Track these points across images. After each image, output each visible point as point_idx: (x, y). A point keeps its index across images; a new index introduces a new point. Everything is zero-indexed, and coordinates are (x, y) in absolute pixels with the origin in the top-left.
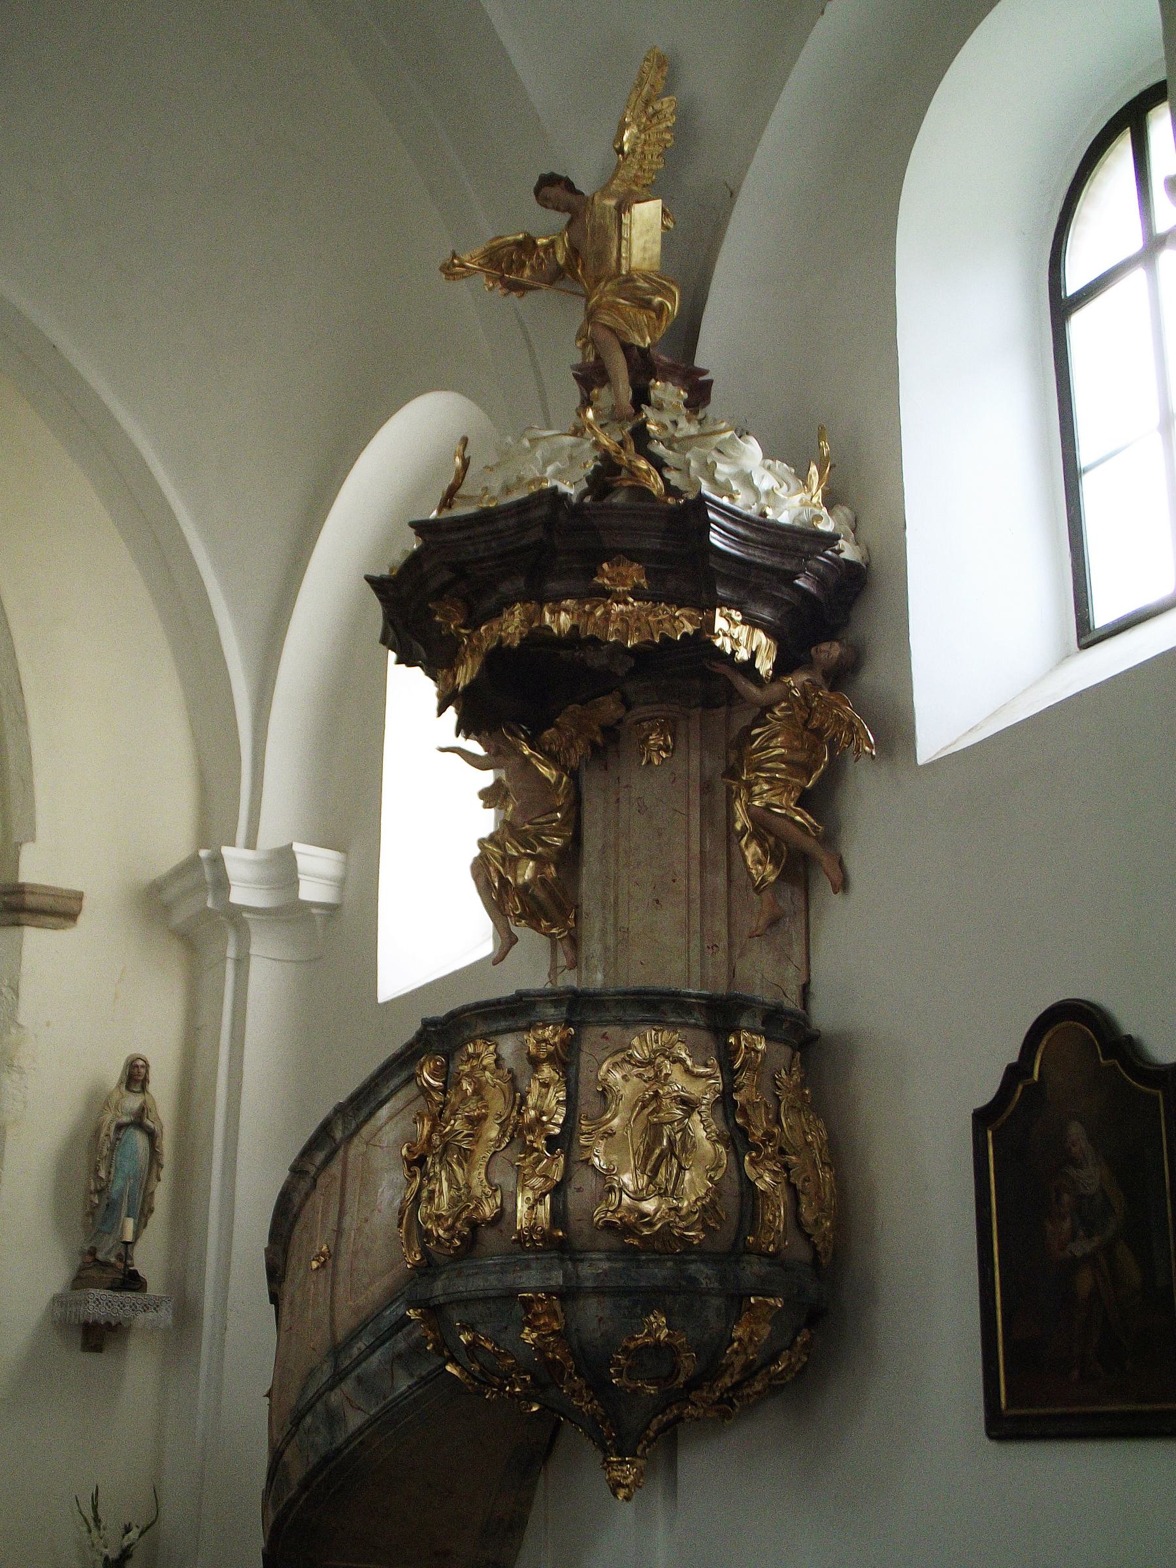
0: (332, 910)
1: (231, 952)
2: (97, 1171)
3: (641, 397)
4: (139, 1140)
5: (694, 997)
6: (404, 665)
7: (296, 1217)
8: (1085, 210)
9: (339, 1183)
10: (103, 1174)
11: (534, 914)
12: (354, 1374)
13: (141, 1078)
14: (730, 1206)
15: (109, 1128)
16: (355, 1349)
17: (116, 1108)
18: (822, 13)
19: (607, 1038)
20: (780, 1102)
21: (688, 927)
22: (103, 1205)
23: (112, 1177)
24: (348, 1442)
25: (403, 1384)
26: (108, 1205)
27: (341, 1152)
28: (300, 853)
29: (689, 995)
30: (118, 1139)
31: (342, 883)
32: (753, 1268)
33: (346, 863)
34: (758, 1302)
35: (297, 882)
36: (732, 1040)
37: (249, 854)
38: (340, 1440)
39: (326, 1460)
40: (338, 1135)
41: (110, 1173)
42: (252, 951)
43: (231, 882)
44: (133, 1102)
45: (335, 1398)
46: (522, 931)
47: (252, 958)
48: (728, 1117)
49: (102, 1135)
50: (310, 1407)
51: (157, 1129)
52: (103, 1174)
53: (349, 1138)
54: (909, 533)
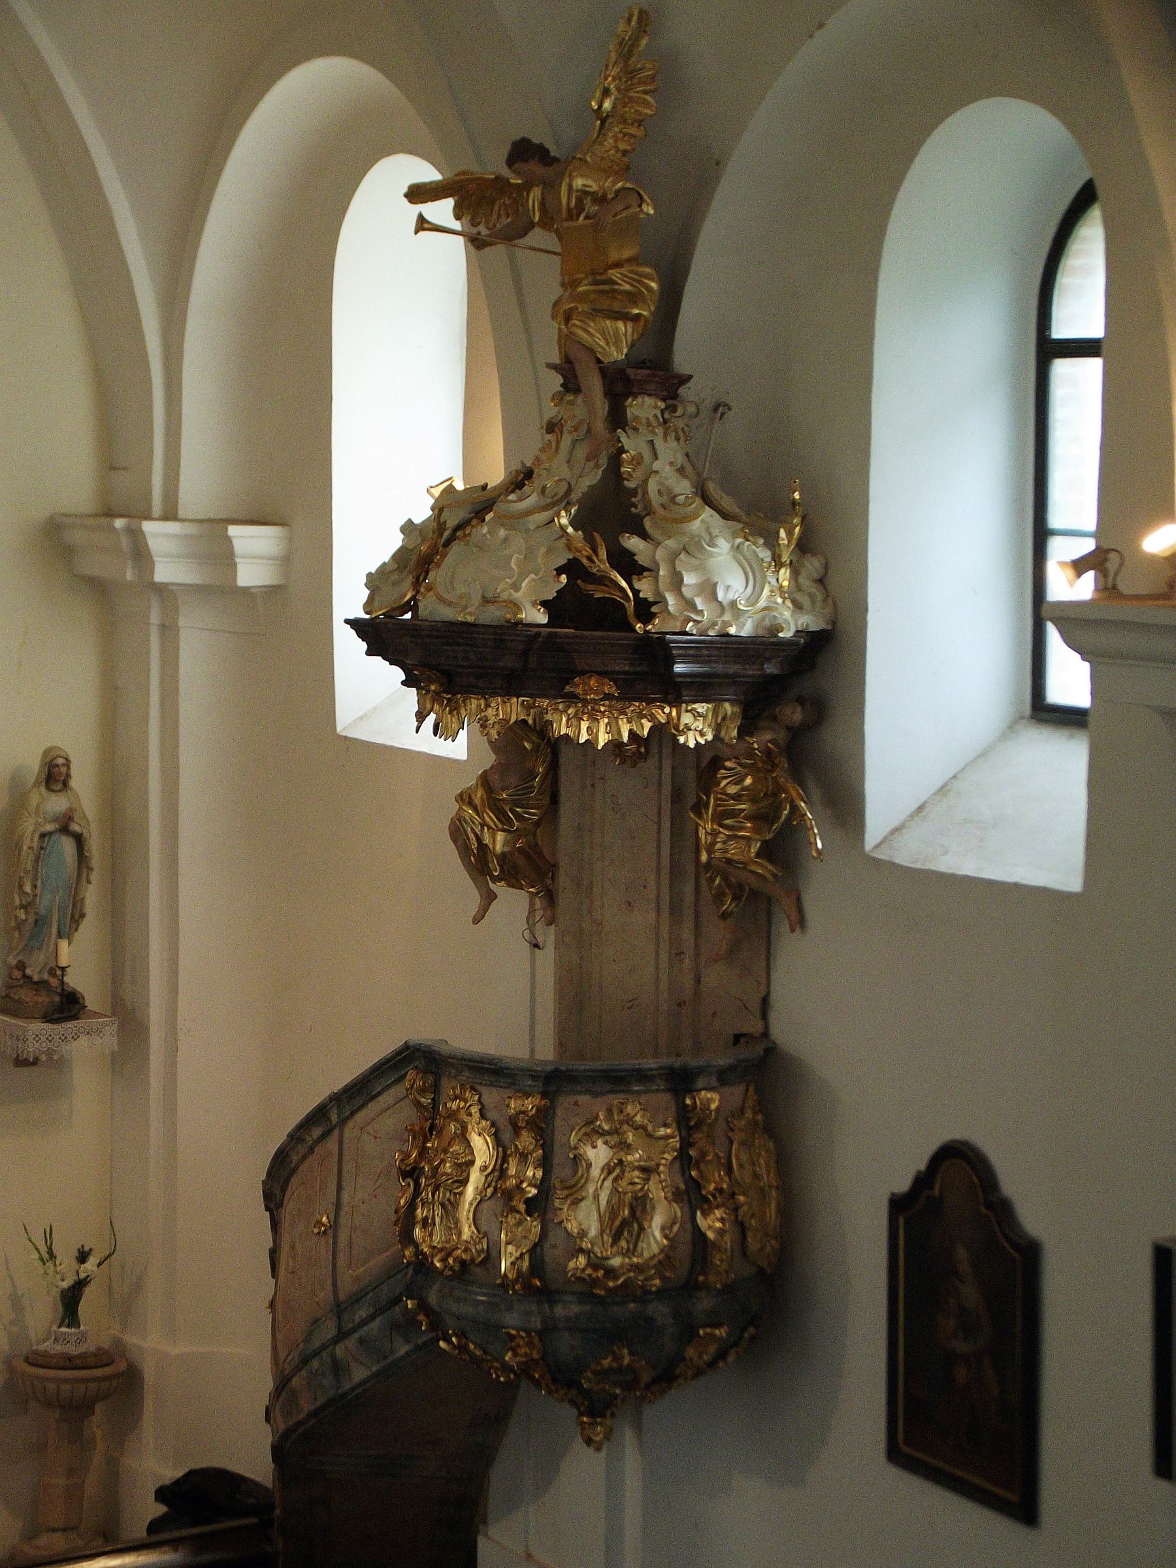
0: (273, 591)
1: (155, 619)
2: (21, 887)
3: (617, 419)
4: (67, 846)
5: (655, 1070)
6: (380, 658)
7: (294, 1171)
8: (1065, 280)
9: (336, 1159)
10: (28, 888)
11: (512, 875)
12: (357, 1335)
13: (62, 778)
14: (684, 1251)
15: (32, 839)
16: (357, 1316)
17: (37, 813)
18: (811, 36)
19: (578, 1106)
20: (731, 1142)
21: (657, 934)
22: (31, 920)
23: (38, 891)
24: (353, 1389)
25: (402, 1349)
26: (36, 922)
27: (336, 1132)
28: (234, 537)
29: (651, 1069)
30: (42, 848)
31: (285, 561)
32: (704, 1303)
33: (290, 539)
34: (706, 1334)
35: (235, 565)
36: (688, 1102)
37: (172, 527)
38: (347, 1386)
39: (331, 1402)
40: (334, 1118)
41: (35, 886)
42: (182, 622)
43: (155, 559)
44: (57, 804)
45: (339, 1350)
46: (499, 888)
47: (181, 631)
48: (684, 1171)
49: (25, 848)
50: (317, 1353)
51: (85, 834)
52: (28, 888)
53: (343, 1122)
54: (871, 617)
